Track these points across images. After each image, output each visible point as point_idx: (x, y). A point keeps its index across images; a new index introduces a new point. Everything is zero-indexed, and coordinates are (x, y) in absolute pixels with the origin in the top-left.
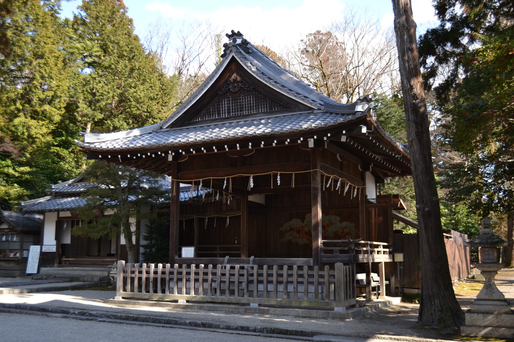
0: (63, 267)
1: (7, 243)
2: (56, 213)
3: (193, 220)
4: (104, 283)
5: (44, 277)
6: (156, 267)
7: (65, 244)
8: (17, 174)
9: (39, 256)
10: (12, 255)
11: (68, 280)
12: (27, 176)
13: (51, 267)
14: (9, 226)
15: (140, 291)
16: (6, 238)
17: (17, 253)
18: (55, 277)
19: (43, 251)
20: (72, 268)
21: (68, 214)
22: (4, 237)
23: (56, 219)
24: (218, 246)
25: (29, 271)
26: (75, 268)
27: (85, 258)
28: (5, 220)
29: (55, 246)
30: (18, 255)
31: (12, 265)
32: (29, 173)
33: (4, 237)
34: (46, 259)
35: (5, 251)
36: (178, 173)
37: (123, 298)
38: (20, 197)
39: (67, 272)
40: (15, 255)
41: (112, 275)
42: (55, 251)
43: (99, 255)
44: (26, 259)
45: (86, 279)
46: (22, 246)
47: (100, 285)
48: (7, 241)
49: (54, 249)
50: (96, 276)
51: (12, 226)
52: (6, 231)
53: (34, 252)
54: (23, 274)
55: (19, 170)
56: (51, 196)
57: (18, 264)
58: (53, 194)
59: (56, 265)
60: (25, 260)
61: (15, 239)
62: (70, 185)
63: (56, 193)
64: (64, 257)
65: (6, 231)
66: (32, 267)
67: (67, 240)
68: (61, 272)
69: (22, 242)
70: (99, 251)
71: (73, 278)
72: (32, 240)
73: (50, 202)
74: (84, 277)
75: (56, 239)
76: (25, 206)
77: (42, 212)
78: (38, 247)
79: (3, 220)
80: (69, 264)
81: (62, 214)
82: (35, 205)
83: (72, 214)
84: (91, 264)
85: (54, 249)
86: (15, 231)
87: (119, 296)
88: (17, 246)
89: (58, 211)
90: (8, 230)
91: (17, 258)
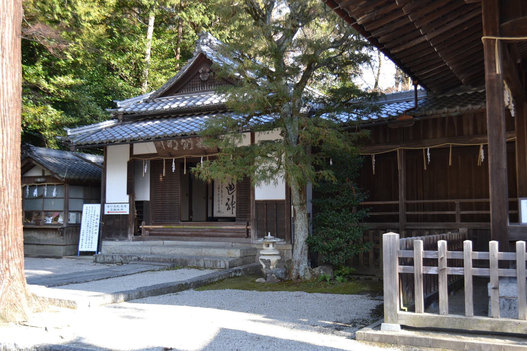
0: (144, 240)
1: (41, 201)
2: (128, 146)
3: (395, 152)
4: (240, 270)
5: (118, 259)
6: (431, 246)
7: (142, 202)
8: (52, 89)
9: (98, 221)
10: (49, 220)
11: (169, 265)
12: (68, 92)
13: (120, 240)
14: (43, 172)
15: (456, 306)
16: (38, 192)
17: (58, 216)
18: (139, 259)
19: (106, 213)
20: (161, 242)
21: (150, 148)
22: (36, 191)
23: (128, 158)
24: (457, 201)
25: (82, 248)
26: (167, 242)
27: (178, 224)
28: (38, 162)
29: (128, 205)
30: (60, 220)
31: (51, 237)
32: (70, 87)
33: (36, 191)
34: (110, 227)
35: (39, 213)
36: (501, 21)
37: (403, 327)
38: (58, 126)
39: (158, 250)
40: (56, 219)
41: (266, 258)
42: (128, 213)
43: (190, 220)
44: (77, 227)
45: (201, 264)
46: (66, 206)
47: (235, 276)
48: (41, 197)
49: (126, 210)
50: (221, 258)
51: (51, 172)
52: (39, 180)
53: (91, 214)
54: (75, 252)
55: (55, 82)
56: (117, 120)
57: (62, 235)
58: (120, 117)
59: (130, 236)
60: (75, 229)
61: (54, 194)
62: (146, 102)
63: (125, 114)
64: (143, 223)
65: (39, 180)
66: (88, 240)
67: (145, 195)
68: (148, 250)
69: (67, 200)
70: (191, 213)
71: (174, 261)
72: (81, 195)
73: (116, 128)
74: (198, 261)
75: (128, 194)
76: (74, 137)
77: (99, 148)
78: (98, 207)
79: (34, 162)
80: (150, 235)
81: (140, 149)
82: (89, 134)
83: (157, 148)
84: (191, 235)
85: (126, 210)
86: (55, 180)
87: (393, 321)
88: (59, 205)
89: (132, 142)
90: (43, 180)
91: (59, 224)
